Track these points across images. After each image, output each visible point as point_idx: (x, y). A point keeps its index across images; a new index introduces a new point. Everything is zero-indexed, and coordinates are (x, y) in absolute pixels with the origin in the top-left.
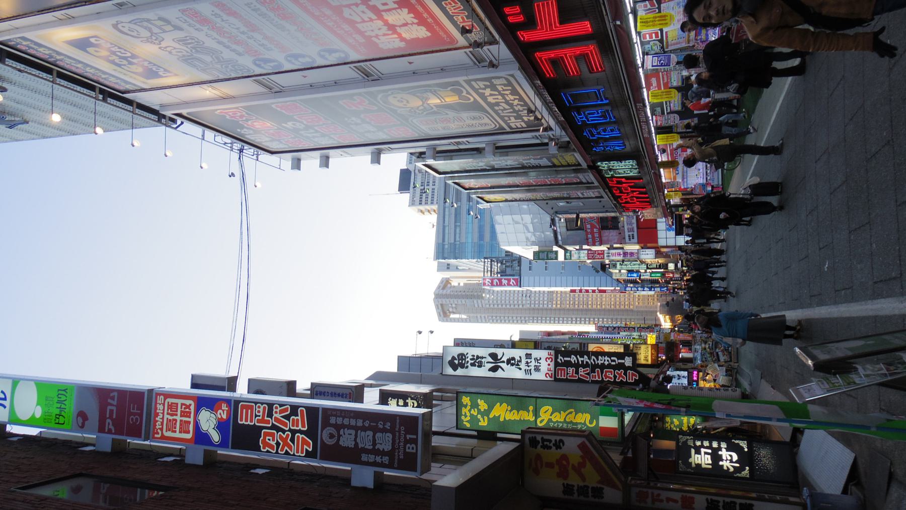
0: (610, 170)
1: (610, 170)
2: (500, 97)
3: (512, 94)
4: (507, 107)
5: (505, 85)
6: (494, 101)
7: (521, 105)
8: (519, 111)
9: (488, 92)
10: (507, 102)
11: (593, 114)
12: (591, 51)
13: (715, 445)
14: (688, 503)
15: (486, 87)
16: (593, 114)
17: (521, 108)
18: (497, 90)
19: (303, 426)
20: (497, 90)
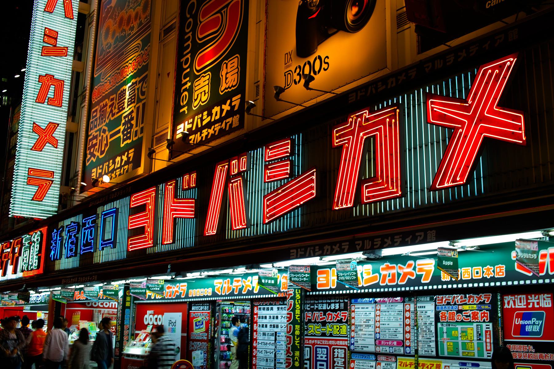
0: (30, 244)
1: (30, 244)
2: (119, 166)
3: (221, 130)
4: (110, 169)
5: (231, 125)
6: (214, 111)
7: (207, 136)
8: (201, 133)
9: (226, 107)
10: (114, 170)
11: (91, 235)
12: (148, 241)
13: (346, 301)
14: (438, 366)
15: (232, 107)
16: (91, 235)
17: (204, 135)
18: (125, 165)
19: (133, 205)
20: (125, 165)
